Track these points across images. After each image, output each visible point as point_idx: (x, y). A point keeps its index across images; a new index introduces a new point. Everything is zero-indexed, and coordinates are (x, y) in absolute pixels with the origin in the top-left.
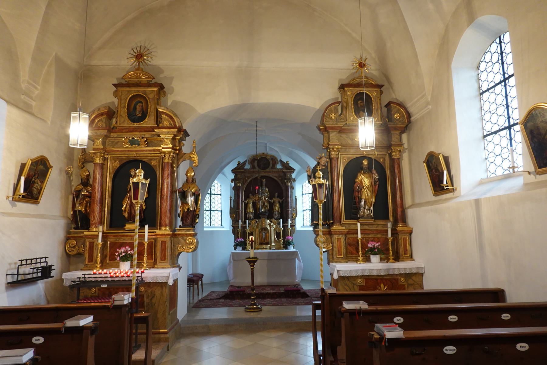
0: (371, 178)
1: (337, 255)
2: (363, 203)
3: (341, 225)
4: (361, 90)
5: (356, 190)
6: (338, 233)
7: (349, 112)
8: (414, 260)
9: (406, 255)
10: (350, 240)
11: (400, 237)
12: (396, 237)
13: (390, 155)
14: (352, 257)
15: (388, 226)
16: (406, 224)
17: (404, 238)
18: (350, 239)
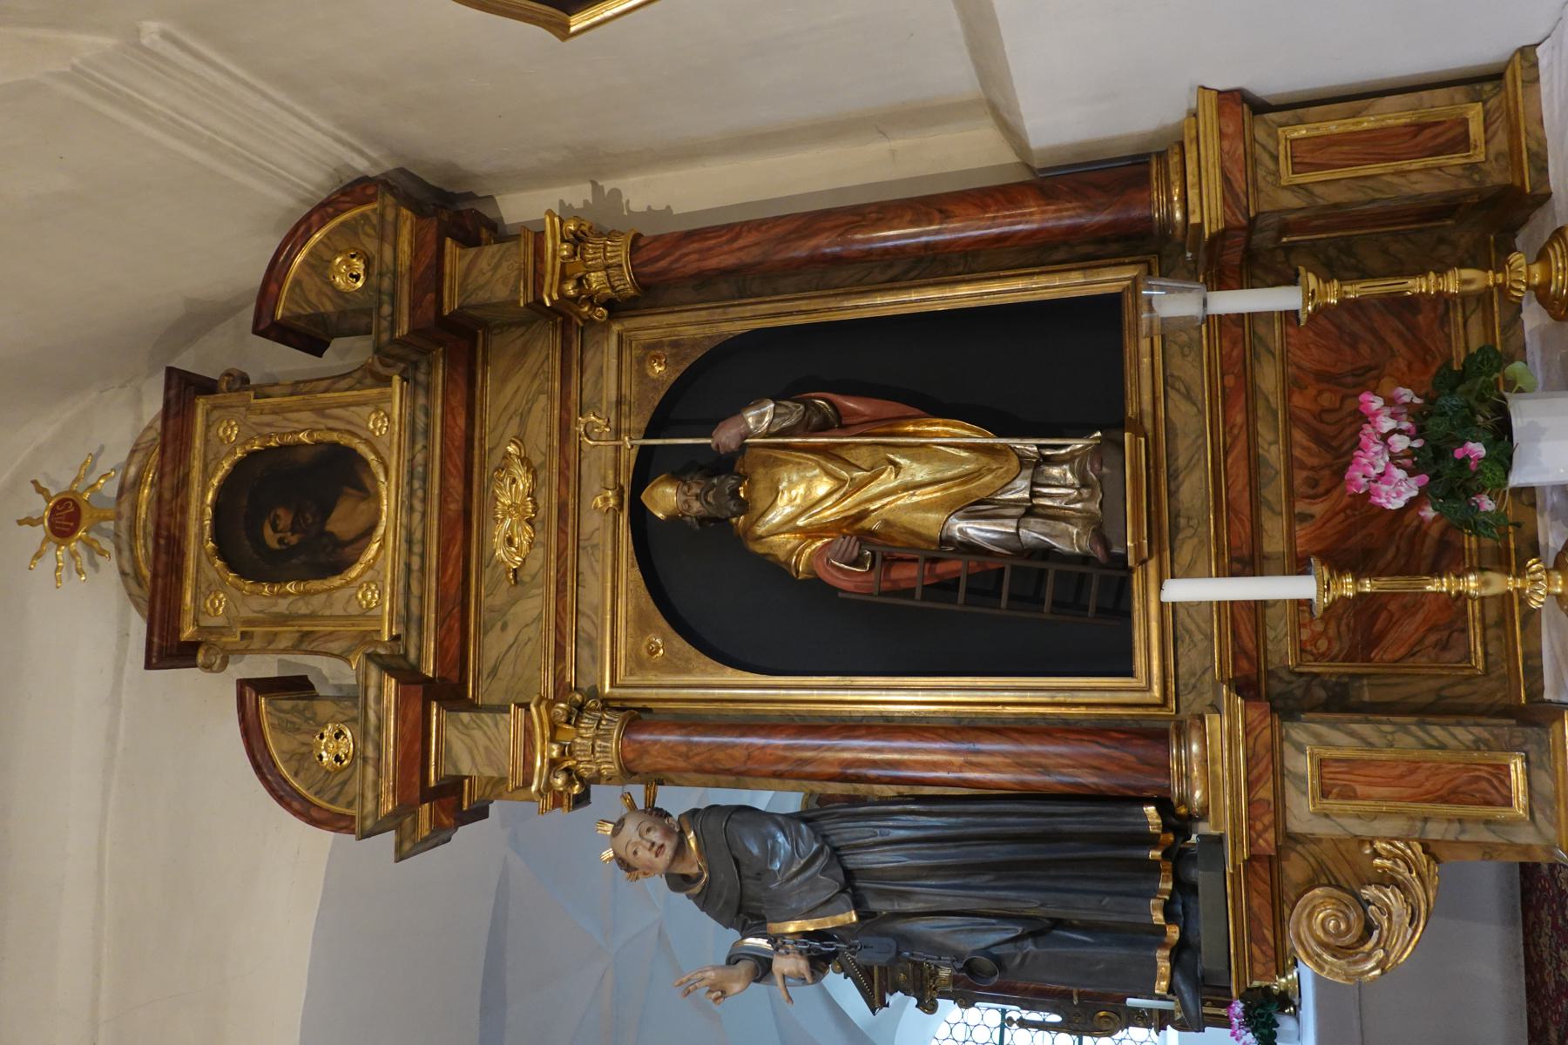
0: (780, 454)
1: (1500, 813)
2: (976, 530)
3: (1182, 732)
4: (202, 528)
5: (872, 577)
6: (1265, 792)
7: (328, 613)
8: (1527, 54)
9: (1476, 129)
10: (1314, 639)
11: (1290, 200)
12: (1285, 229)
13: (617, 307)
14: (1484, 629)
15: (1192, 319)
16: (1162, 156)
17: (1299, 166)
18: (1305, 634)
